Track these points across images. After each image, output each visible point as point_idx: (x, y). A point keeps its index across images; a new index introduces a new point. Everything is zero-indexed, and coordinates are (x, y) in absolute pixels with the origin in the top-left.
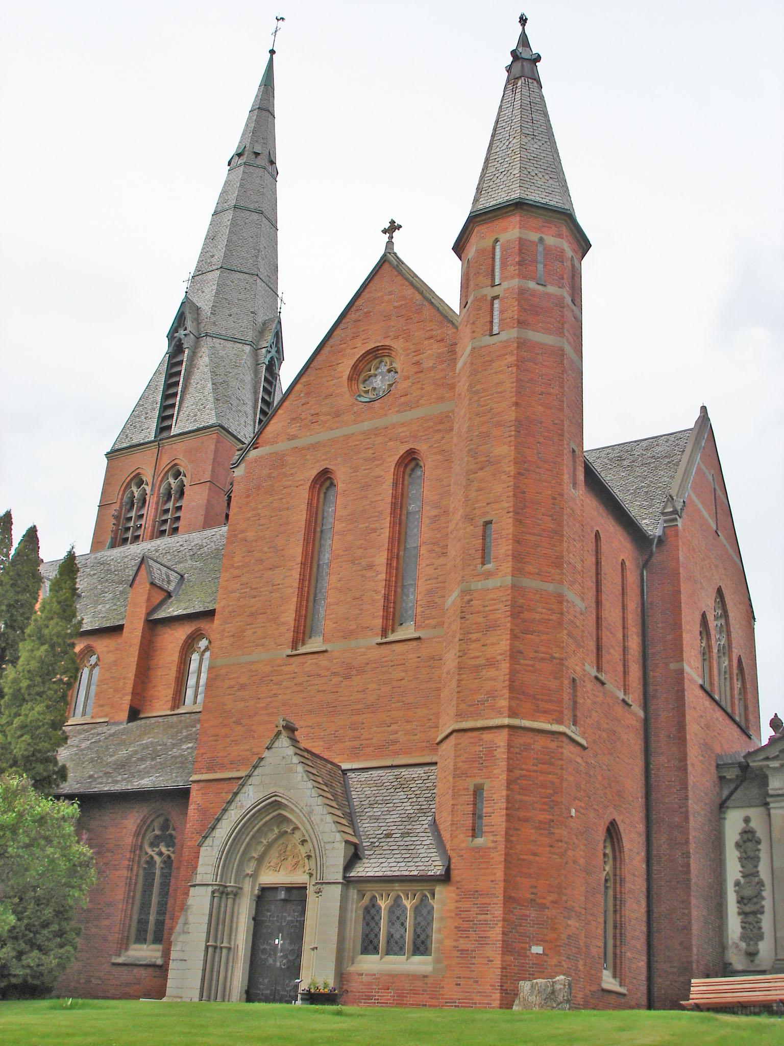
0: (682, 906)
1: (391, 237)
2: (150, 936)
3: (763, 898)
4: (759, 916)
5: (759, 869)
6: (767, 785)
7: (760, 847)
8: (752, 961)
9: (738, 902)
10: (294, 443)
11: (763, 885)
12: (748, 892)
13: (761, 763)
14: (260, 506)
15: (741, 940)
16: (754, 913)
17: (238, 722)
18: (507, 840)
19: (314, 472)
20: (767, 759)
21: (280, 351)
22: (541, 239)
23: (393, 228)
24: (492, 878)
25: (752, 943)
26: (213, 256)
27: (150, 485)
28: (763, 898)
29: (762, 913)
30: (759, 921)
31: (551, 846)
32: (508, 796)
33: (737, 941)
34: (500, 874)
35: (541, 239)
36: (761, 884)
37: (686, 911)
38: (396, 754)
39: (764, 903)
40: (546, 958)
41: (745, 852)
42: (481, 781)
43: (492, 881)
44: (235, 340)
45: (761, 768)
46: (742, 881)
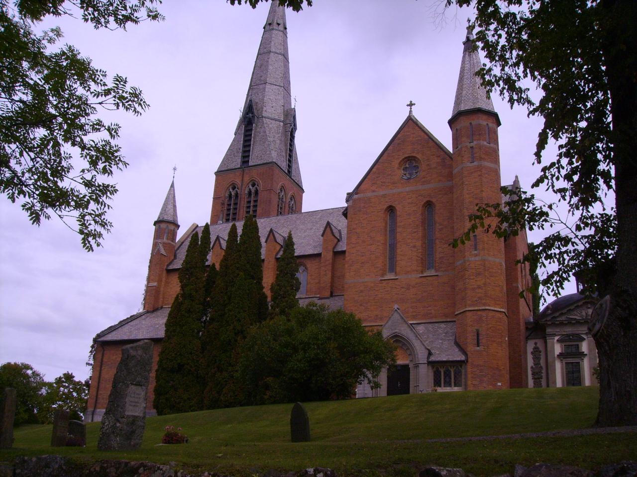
1: (411, 109)
2: (453, 384)
3: (542, 373)
4: (541, 380)
7: (541, 354)
9: (532, 374)
10: (375, 194)
11: (542, 368)
14: (361, 219)
16: (539, 378)
17: (361, 305)
19: (385, 207)
21: (295, 125)
22: (487, 124)
23: (411, 105)
26: (261, 76)
27: (240, 189)
35: (487, 124)
36: (541, 367)
37: (520, 376)
38: (432, 318)
39: (542, 375)
44: (276, 120)
46: (534, 366)
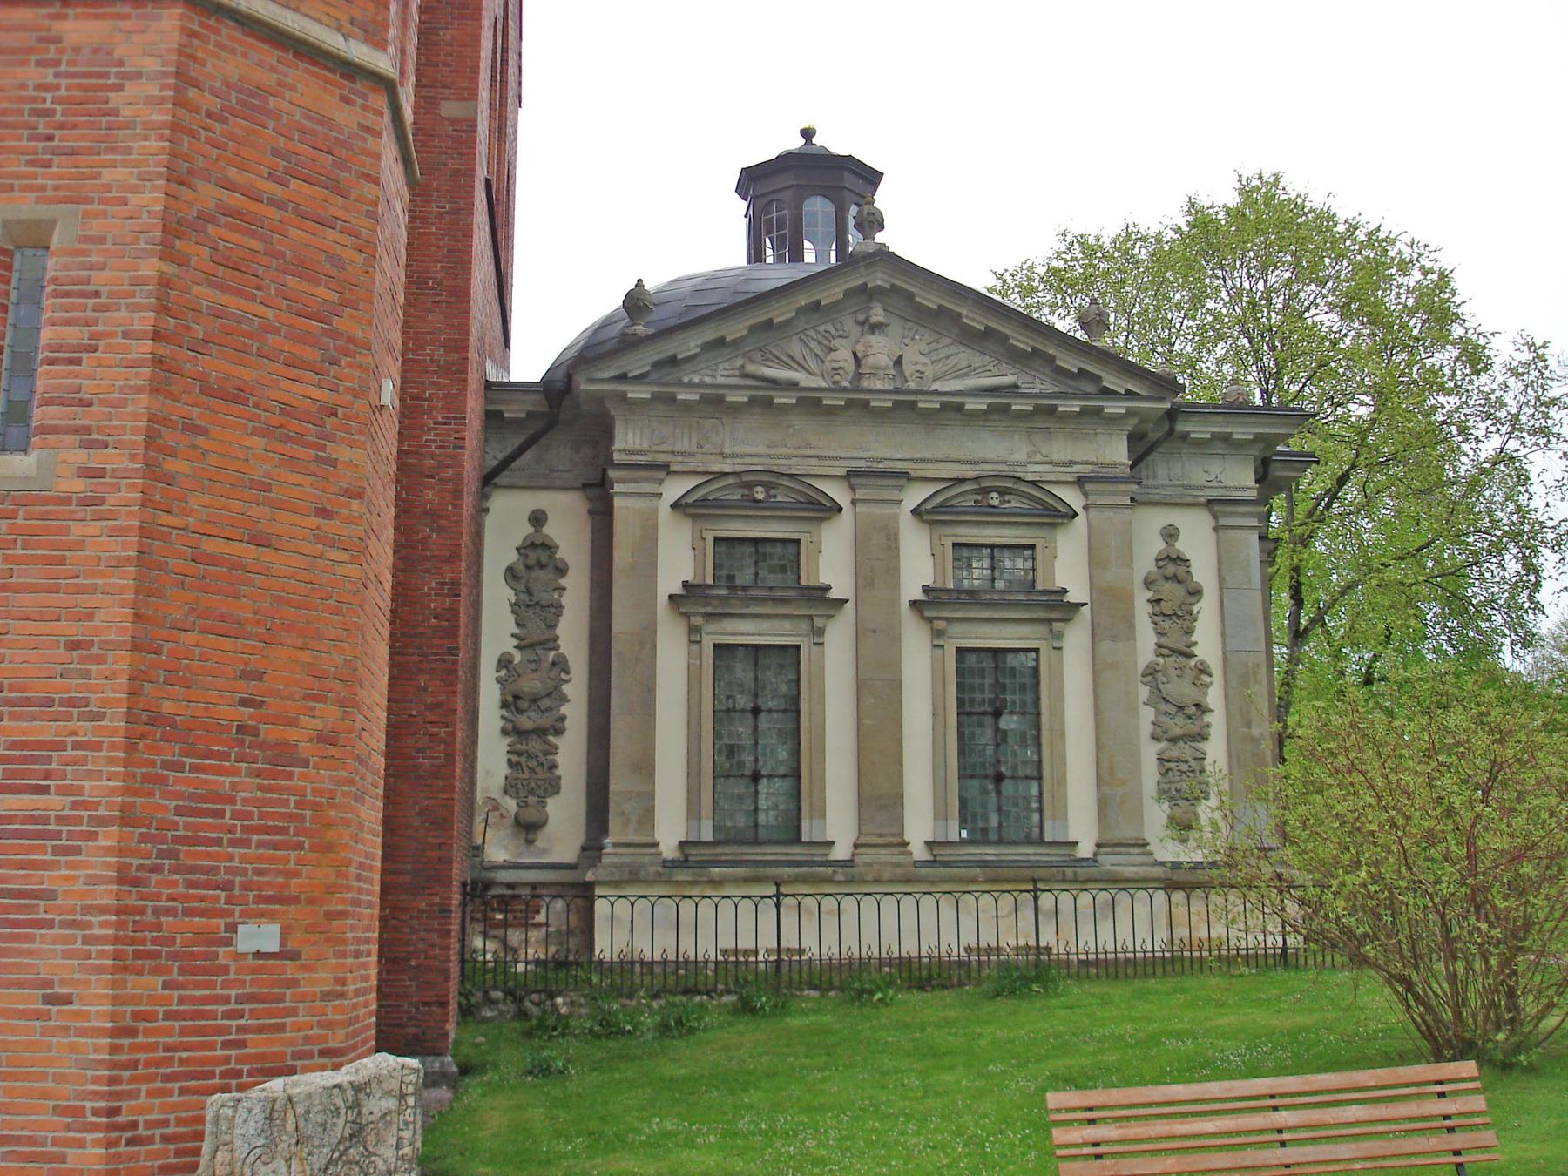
0: (430, 716)
3: (564, 699)
5: (558, 631)
6: (610, 439)
7: (563, 582)
8: (530, 842)
9: (504, 705)
12: (531, 684)
13: (606, 387)
15: (506, 792)
16: (541, 732)
18: (151, 471)
20: (622, 377)
24: (75, 630)
25: (532, 800)
28: (564, 699)
29: (559, 732)
30: (554, 750)
31: (324, 513)
32: (165, 283)
33: (496, 794)
34: (112, 617)
36: (561, 664)
40: (290, 969)
41: (529, 593)
42: (42, 211)
43: (74, 645)
45: (599, 399)
46: (517, 657)
